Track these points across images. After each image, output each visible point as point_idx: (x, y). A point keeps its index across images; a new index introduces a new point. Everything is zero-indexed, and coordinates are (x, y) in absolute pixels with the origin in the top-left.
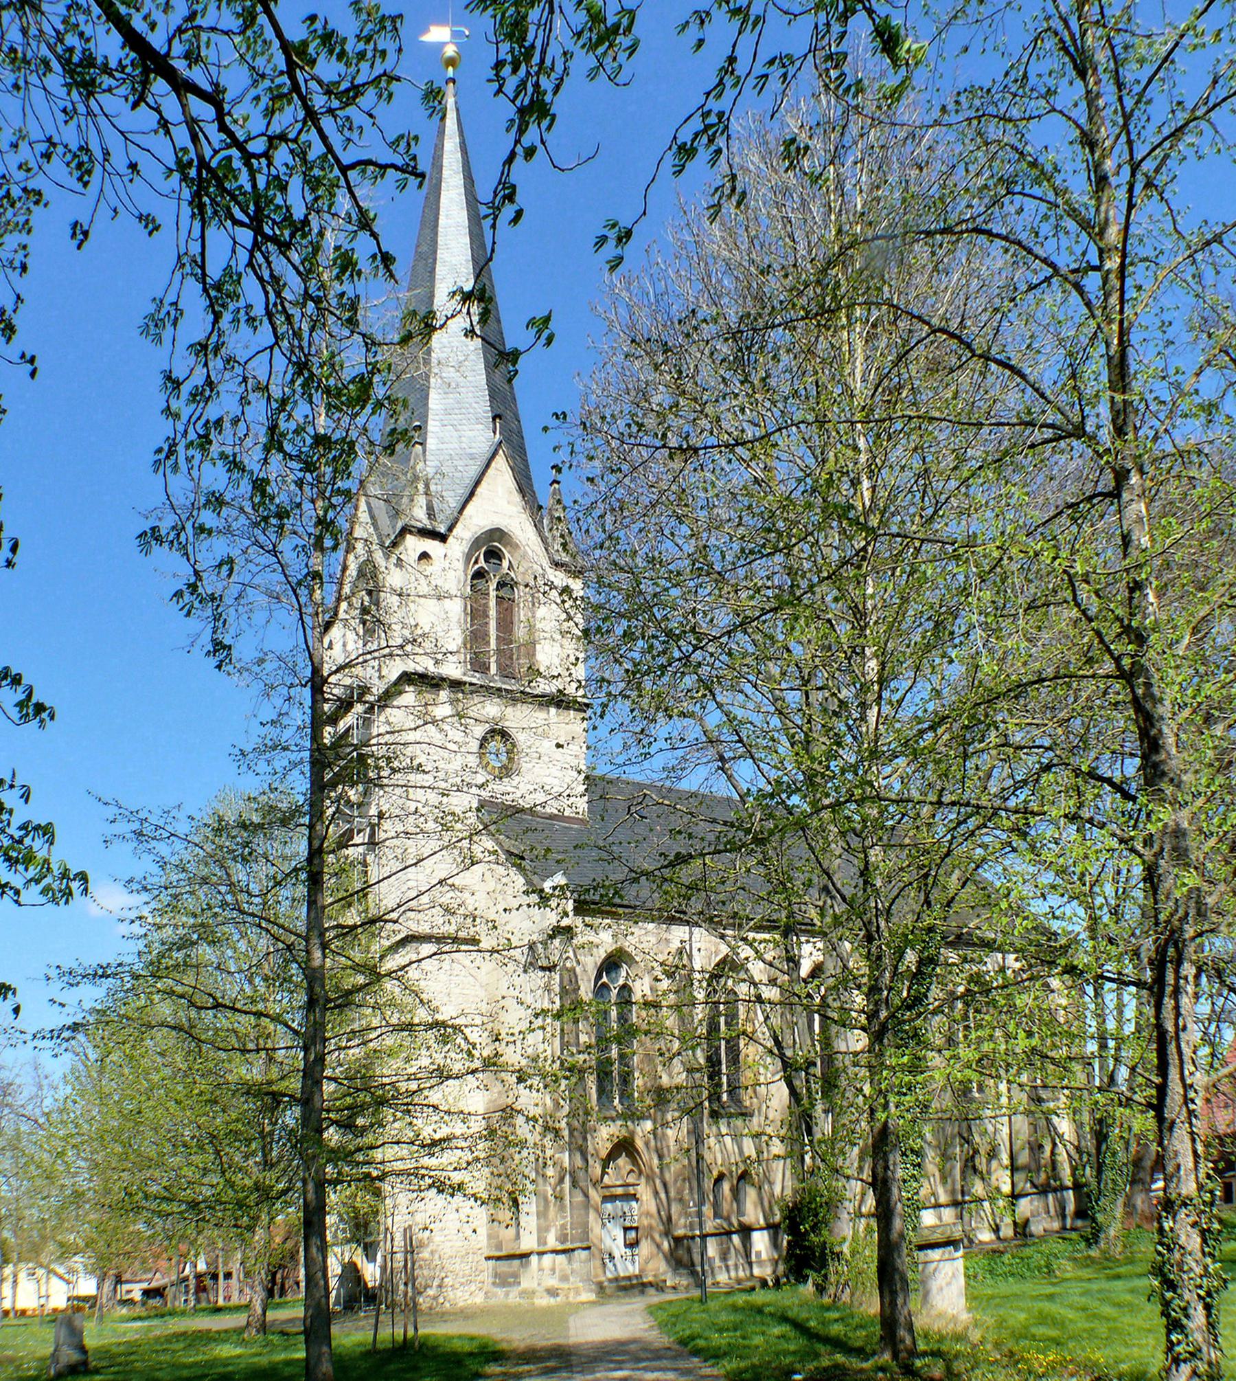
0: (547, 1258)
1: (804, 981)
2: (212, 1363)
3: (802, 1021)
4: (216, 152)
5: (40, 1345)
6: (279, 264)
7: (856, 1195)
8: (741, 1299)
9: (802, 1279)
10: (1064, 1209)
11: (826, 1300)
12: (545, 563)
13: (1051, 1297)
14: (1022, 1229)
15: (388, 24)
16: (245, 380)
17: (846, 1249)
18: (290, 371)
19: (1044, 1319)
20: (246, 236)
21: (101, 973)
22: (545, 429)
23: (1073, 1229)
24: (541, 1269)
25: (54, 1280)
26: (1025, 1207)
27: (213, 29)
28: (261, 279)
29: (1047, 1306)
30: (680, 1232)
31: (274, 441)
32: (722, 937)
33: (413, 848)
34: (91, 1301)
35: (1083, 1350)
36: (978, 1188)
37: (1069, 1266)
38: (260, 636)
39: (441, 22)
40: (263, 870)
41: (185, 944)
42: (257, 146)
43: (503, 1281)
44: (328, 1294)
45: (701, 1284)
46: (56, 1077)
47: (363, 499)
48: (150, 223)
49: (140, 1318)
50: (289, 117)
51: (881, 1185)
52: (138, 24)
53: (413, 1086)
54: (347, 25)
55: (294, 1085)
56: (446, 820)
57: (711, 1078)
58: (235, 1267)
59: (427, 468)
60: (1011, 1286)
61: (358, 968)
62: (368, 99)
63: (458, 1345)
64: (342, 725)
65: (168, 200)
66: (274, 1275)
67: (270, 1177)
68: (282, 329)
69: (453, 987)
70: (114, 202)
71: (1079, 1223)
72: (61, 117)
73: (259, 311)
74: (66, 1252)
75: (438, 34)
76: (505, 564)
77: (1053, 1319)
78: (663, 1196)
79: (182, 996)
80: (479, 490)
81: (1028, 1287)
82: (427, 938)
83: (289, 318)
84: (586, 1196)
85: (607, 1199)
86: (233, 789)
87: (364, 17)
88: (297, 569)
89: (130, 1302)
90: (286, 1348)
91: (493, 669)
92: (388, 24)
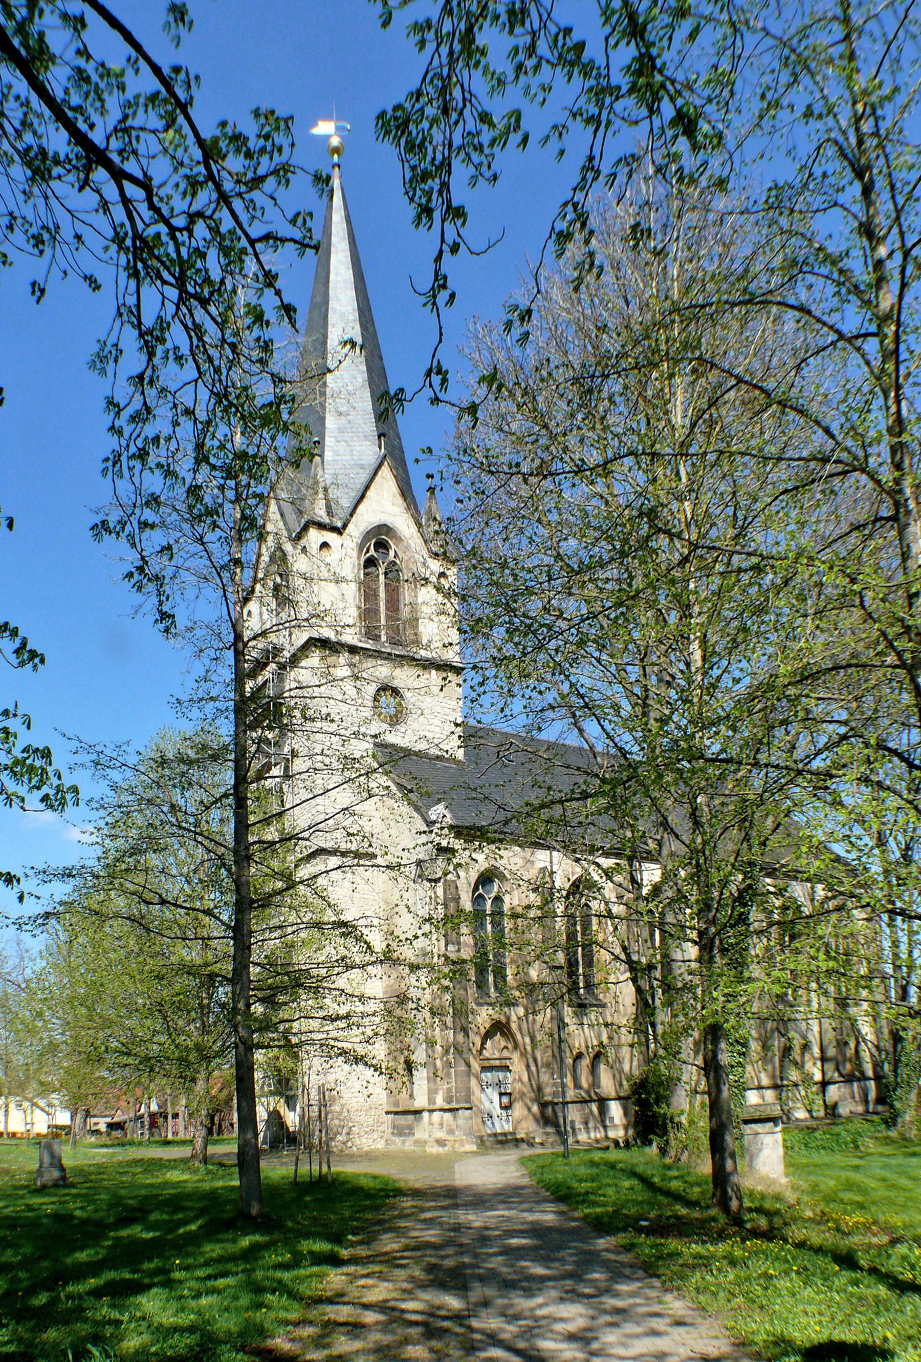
0: (436, 1115)
1: (646, 899)
2: (167, 1184)
3: (646, 933)
4: (147, 226)
5: (28, 1161)
6: (200, 314)
7: (691, 1074)
8: (597, 1156)
9: (648, 1142)
10: (866, 1096)
11: (668, 1161)
12: (425, 553)
13: (856, 1168)
14: (832, 1110)
15: (282, 124)
16: (175, 406)
17: (684, 1119)
18: (213, 401)
19: (850, 1186)
20: (172, 293)
21: (68, 874)
22: (417, 461)
23: (875, 1113)
24: (431, 1124)
25: (37, 1112)
26: (833, 1092)
27: (142, 129)
28: (186, 326)
29: (852, 1175)
30: (548, 1098)
31: (201, 457)
32: (577, 860)
33: (320, 781)
34: (67, 1129)
35: (884, 1213)
36: (794, 1075)
37: (871, 1143)
38: (191, 608)
39: (328, 117)
40: (195, 795)
41: (135, 851)
42: (180, 221)
43: (400, 1131)
44: (256, 1135)
45: (564, 1142)
46: (35, 952)
47: (273, 502)
48: (93, 283)
49: (106, 1146)
50: (205, 197)
51: (712, 1069)
52: (82, 126)
53: (323, 972)
54: (249, 128)
55: (227, 967)
56: (349, 761)
57: (570, 976)
58: (181, 1110)
59: (325, 476)
60: (824, 1157)
61: (276, 875)
62: (270, 184)
63: (364, 1182)
64: (260, 680)
65: (111, 269)
66: (212, 1118)
67: (208, 1039)
68: (205, 366)
69: (357, 895)
70: (64, 265)
71: (880, 1108)
72: (21, 197)
73: (185, 350)
74: (46, 1089)
75: (325, 128)
76: (392, 553)
77: (858, 1186)
78: (533, 1068)
79: (133, 894)
80: (368, 493)
81: (839, 1158)
82: (334, 852)
83: (210, 360)
84: (468, 1065)
85: (484, 1069)
86: (174, 731)
87: (263, 120)
88: (220, 555)
89: (97, 1132)
90: (222, 1178)
91: (384, 638)
92: (282, 124)
